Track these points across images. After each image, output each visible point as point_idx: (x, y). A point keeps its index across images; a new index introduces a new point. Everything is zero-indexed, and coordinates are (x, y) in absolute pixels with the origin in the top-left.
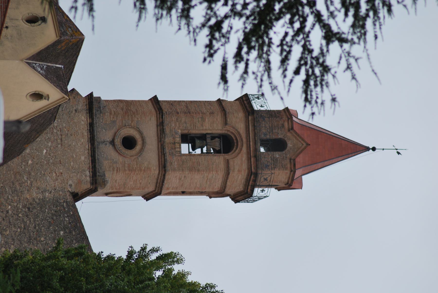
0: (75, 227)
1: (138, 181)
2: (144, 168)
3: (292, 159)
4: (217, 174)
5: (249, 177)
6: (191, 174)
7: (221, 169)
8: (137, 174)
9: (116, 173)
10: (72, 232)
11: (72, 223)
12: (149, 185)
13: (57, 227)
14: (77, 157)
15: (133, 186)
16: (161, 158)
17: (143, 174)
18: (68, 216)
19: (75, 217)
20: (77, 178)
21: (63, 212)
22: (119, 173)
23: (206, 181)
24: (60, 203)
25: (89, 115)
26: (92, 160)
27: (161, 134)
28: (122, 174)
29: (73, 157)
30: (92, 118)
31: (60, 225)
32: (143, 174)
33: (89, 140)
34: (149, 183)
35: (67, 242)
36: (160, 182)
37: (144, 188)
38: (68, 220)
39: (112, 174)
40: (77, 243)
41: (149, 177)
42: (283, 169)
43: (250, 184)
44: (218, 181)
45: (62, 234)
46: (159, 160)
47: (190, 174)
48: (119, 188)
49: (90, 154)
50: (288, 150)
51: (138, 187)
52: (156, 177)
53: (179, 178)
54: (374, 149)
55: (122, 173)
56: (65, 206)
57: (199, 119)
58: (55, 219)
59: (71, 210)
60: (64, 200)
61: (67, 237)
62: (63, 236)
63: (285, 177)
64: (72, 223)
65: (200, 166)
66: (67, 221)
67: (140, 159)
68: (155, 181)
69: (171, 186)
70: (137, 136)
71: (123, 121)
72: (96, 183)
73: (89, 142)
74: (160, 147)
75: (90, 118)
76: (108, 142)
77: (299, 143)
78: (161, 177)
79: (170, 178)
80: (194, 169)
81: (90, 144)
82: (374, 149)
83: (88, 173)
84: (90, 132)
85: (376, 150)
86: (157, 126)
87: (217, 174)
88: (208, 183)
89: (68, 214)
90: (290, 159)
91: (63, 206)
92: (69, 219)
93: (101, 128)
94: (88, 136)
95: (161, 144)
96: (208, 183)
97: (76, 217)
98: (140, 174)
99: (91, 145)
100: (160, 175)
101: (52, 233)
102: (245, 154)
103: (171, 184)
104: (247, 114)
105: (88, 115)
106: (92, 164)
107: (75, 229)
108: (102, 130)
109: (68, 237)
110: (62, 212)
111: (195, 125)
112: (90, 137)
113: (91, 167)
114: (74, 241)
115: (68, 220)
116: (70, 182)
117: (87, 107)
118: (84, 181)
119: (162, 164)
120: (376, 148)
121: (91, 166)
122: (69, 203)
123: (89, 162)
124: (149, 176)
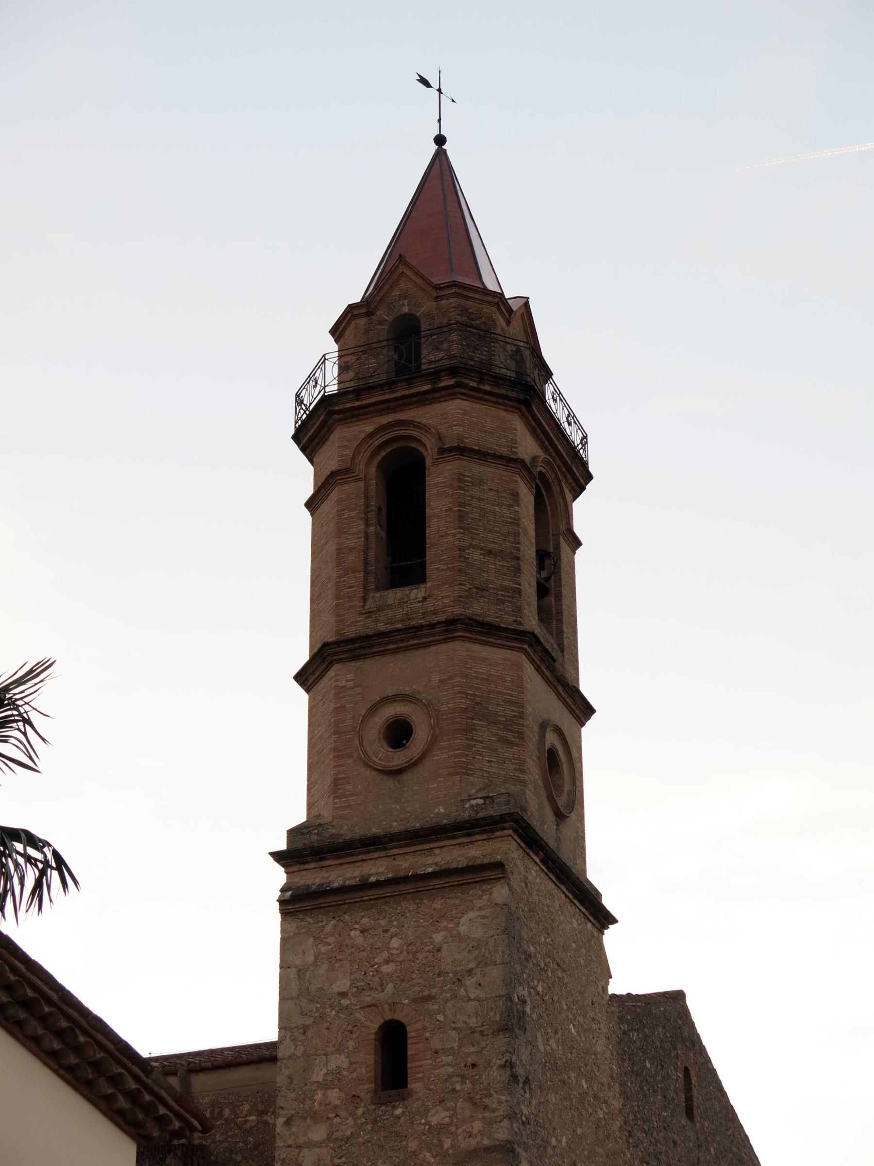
54: (440, 140)
82: (440, 140)
85: (442, 133)
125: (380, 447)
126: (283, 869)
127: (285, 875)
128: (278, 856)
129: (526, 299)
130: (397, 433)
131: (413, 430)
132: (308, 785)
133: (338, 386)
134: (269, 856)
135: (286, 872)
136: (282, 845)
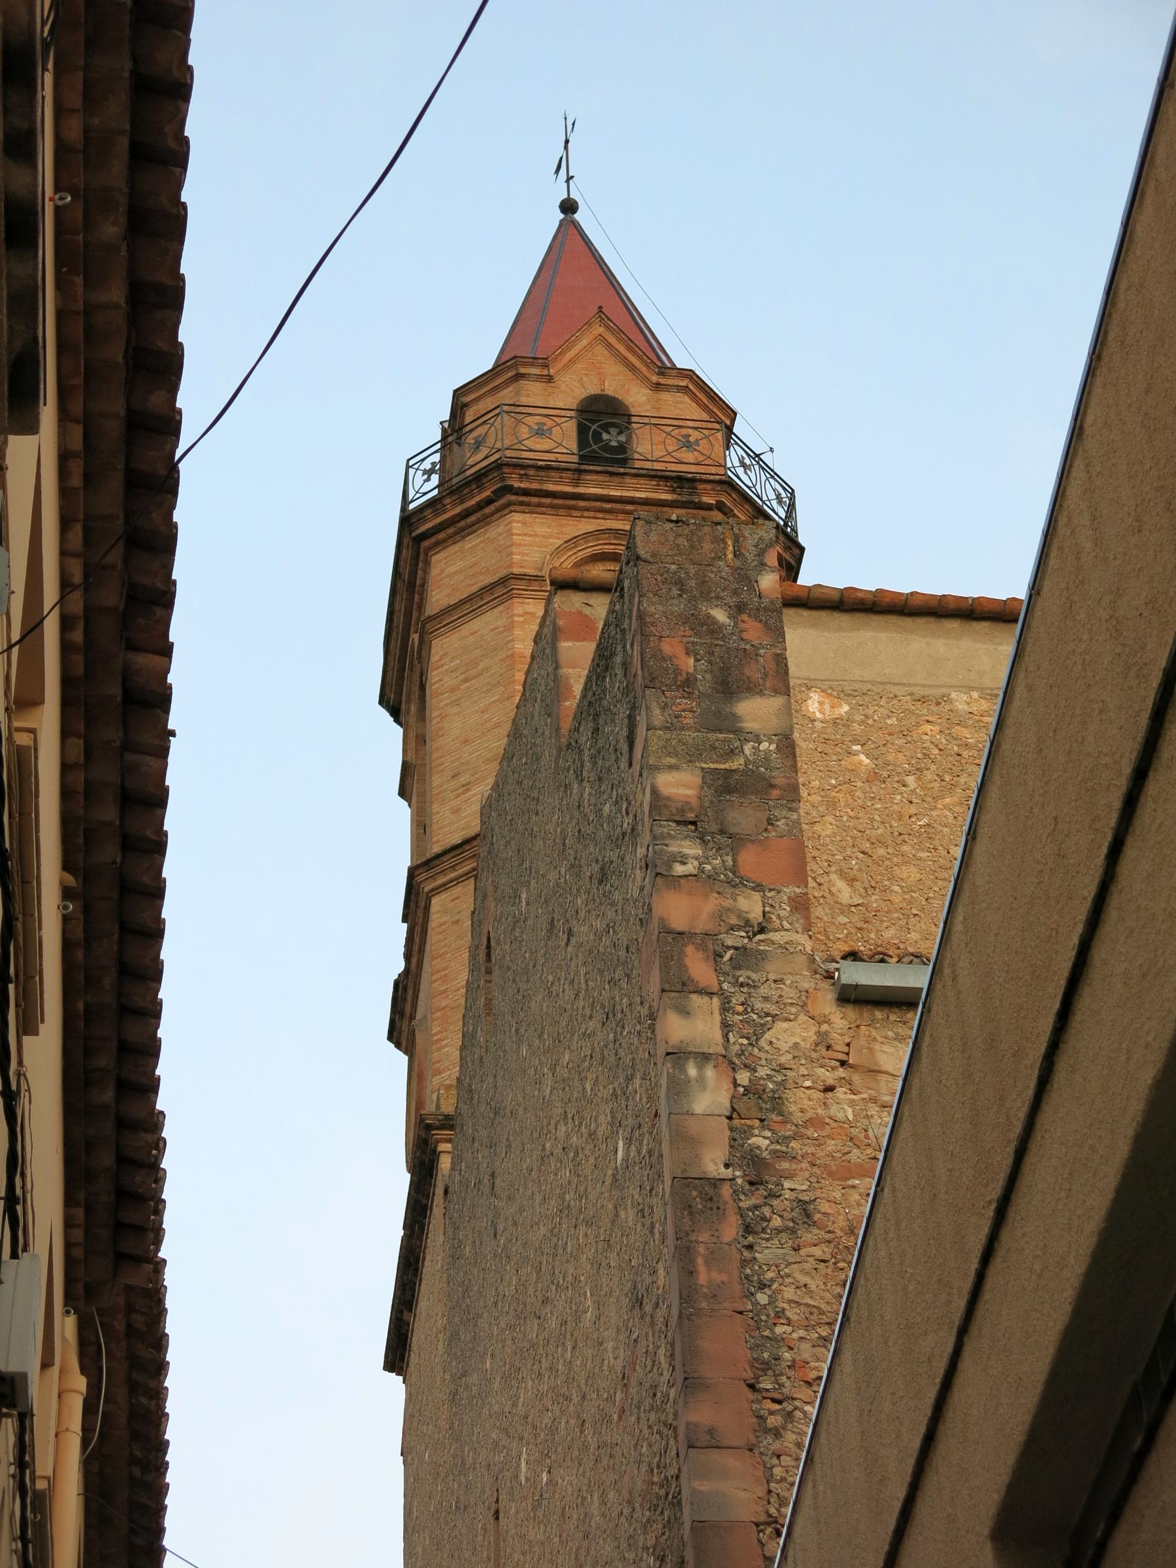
5: (441, 536)
17: (447, 953)
53: (463, 793)
54: (569, 207)
82: (569, 207)
98: (446, 969)
120: (566, 196)
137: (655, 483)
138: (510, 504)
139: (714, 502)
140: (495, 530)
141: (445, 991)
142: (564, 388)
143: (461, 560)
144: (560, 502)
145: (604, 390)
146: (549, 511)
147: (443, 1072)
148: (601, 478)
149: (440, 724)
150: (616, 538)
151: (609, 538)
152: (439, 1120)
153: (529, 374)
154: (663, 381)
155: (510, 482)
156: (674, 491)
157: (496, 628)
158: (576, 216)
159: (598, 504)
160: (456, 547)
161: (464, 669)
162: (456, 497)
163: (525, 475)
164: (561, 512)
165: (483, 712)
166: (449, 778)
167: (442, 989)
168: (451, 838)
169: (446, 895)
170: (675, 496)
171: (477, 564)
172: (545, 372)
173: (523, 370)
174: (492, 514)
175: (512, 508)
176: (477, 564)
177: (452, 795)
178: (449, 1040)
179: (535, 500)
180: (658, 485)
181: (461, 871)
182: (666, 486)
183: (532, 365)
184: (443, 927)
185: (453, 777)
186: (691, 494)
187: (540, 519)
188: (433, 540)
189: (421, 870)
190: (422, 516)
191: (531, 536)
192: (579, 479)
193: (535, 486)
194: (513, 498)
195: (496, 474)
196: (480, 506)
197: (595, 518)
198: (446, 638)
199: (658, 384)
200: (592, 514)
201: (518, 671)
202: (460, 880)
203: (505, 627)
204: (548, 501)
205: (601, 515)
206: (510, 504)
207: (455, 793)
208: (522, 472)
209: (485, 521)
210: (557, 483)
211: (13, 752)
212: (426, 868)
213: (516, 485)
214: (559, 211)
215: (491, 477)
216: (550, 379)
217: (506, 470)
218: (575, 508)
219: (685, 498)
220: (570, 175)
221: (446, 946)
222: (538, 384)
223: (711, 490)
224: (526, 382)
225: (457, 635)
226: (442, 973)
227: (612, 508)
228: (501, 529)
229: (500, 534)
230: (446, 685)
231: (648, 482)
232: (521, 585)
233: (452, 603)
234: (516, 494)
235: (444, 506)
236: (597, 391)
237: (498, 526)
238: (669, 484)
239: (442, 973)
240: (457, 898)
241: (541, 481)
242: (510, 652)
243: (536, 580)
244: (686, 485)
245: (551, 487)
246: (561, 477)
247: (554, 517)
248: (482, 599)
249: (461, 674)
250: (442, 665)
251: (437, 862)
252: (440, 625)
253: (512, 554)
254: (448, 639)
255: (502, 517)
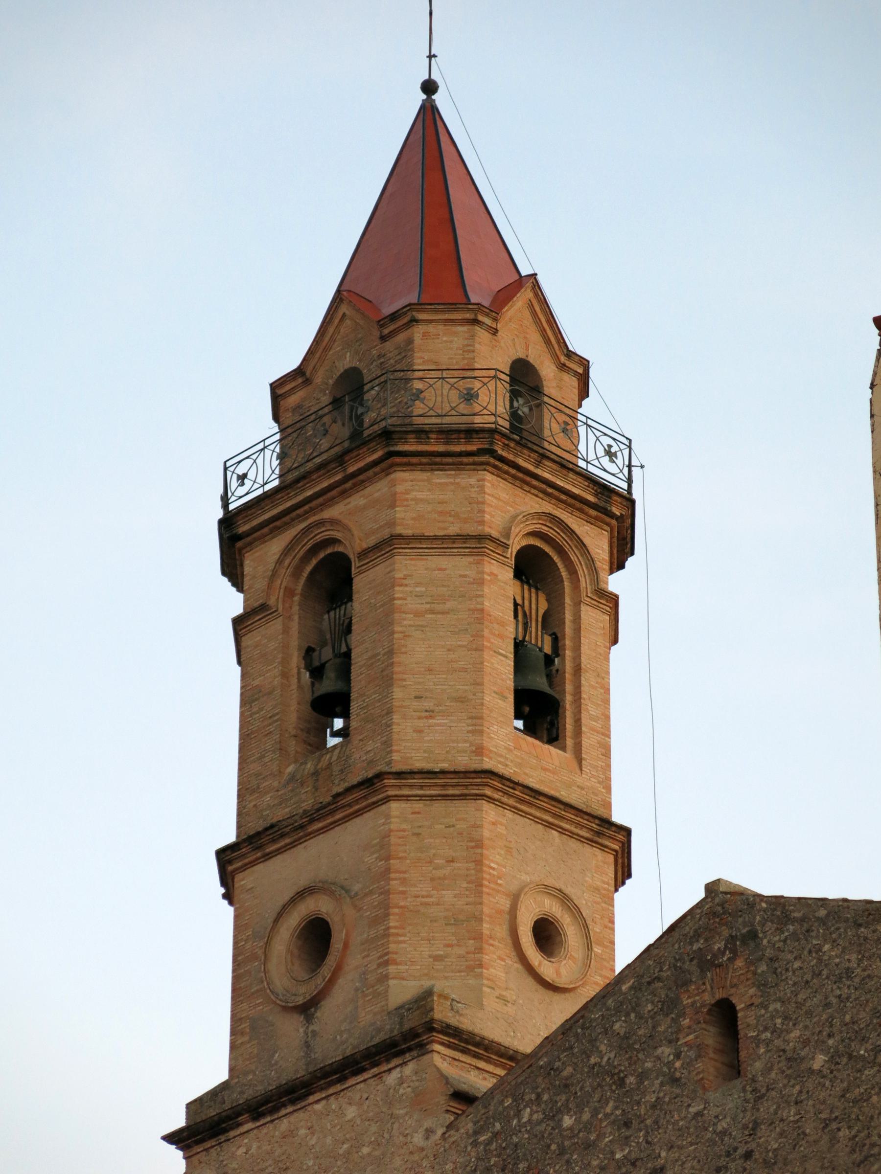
0: (549, 1074)
1: (440, 873)
2: (381, 860)
3: (381, 332)
4: (405, 582)
5: (414, 460)
6: (406, 676)
7: (388, 570)
8: (404, 881)
9: (396, 964)
10: (567, 1079)
11: (537, 1088)
12: (461, 826)
13: (549, 1146)
14: (348, 1136)
15: (465, 885)
16: (350, 805)
17: (406, 858)
18: (518, 1114)
19: (521, 1083)
20: (406, 1114)
21: (505, 1140)
22: (396, 953)
23: (443, 613)
24: (478, 1159)
25: (232, 1129)
26: (356, 1073)
27: (283, 836)
28: (404, 942)
29: (348, 1152)
30: (237, 1117)
31: (543, 1136)
32: (406, 858)
33: (299, 1106)
34: (452, 829)
35: (594, 1089)
36: (436, 785)
37: (473, 844)
38: (528, 1110)
39: (403, 979)
40: (598, 1048)
41: (418, 834)
42: (409, 353)
43: (441, 448)
44: (440, 569)
45: (571, 1116)
46: (357, 811)
47: (405, 680)
48: (471, 942)
49: (339, 1087)
50: (360, 360)
51: (472, 865)
52: (419, 806)
53: (426, 717)
54: (429, 87)
55: (395, 942)
56: (490, 1134)
57: (255, 710)
58: (526, 1165)
59: (501, 1109)
60: (469, 1148)
61: (579, 1094)
62: (575, 1113)
63: (445, 339)
64: (540, 1090)
65: (378, 654)
66: (532, 1110)
67: (356, 887)
68: (439, 807)
69: (465, 741)
70: (294, 920)
71: (253, 994)
72: (413, 1034)
73: (303, 1104)
74: (320, 825)
75: (239, 1125)
76: (307, 1028)
77: (342, 331)
78: (411, 786)
79: (425, 752)
80: (385, 673)
81: (311, 1099)
82: (429, 87)
83: (392, 1078)
84: (276, 1109)
85: (433, 77)
86: (268, 857)
87: (405, 582)
88: (449, 605)
89: (512, 1113)
90: (383, 338)
91: (488, 1143)
92: (525, 1107)
93: (268, 1072)
94: (291, 1113)
95: (312, 821)
96: (449, 605)
97: (519, 1080)
98: (404, 872)
99: (312, 1094)
100: (405, 792)
101: (568, 1162)
102: (349, 503)
103: (453, 741)
104: (239, 544)
105: (232, 1134)
106: (363, 1070)
107: (557, 1069)
108: (276, 1063)
109: (581, 1089)
110: (504, 1145)
111: (270, 717)
112: (293, 1102)
113: (375, 1070)
114: (593, 1060)
115: (528, 1110)
116: (418, 1139)
117: (213, 1147)
118: (417, 1084)
119: (365, 797)
120: (427, 77)
121: (372, 1071)
122: (478, 1122)
123: (362, 1085)
124: (414, 834)
125: (306, 558)
126: (180, 1154)
127: (184, 1161)
128: (172, 1138)
129: (532, 280)
130: (319, 538)
131: (332, 530)
132: (239, 791)
133: (281, 435)
134: (165, 1144)
135: (185, 1158)
136: (179, 1121)
137: (587, 484)
138: (488, 464)
139: (619, 514)
140: (468, 479)
141: (403, 893)
142: (502, 344)
143: (429, 490)
144: (521, 475)
145: (527, 356)
146: (510, 479)
147: (400, 964)
148: (555, 466)
149: (403, 641)
150: (551, 522)
151: (545, 521)
152: (442, 1027)
153: (483, 323)
154: (568, 363)
155: (496, 448)
156: (596, 495)
157: (465, 576)
158: (434, 97)
159: (544, 486)
160: (425, 475)
161: (429, 600)
162: (444, 436)
163: (507, 445)
164: (517, 483)
165: (449, 650)
166: (412, 697)
167: (401, 889)
168: (413, 755)
169: (407, 805)
170: (596, 500)
171: (446, 503)
172: (494, 326)
173: (480, 318)
174: (467, 464)
175: (488, 468)
176: (446, 503)
177: (414, 713)
178: (406, 939)
179: (506, 467)
180: (588, 487)
181: (428, 792)
182: (593, 489)
183: (487, 315)
184: (403, 833)
185: (415, 698)
186: (606, 502)
187: (502, 484)
188: (405, 460)
189: (391, 776)
190: (405, 436)
191: (496, 498)
192: (540, 462)
193: (511, 457)
194: (492, 460)
195: (487, 436)
196: (461, 454)
197: (537, 496)
198: (411, 559)
199: (564, 365)
200: (536, 492)
201: (487, 628)
202: (424, 798)
203: (474, 579)
204: (513, 471)
205: (541, 495)
206: (488, 464)
207: (418, 714)
208: (507, 442)
209: (459, 467)
210: (525, 460)
211: (555, 815)
212: (395, 776)
213: (500, 452)
214: (420, 86)
215: (481, 436)
216: (495, 332)
217: (497, 437)
218: (528, 484)
219: (602, 504)
220: (432, 54)
221: (405, 851)
222: (486, 334)
223: (621, 503)
224: (479, 329)
225: (423, 563)
226: (402, 875)
227: (552, 493)
228: (473, 481)
229: (472, 486)
230: (410, 606)
231: (582, 481)
232: (491, 546)
233: (426, 534)
234: (494, 458)
235: (428, 438)
236: (524, 357)
237: (470, 477)
238: (595, 488)
239: (402, 875)
240: (419, 813)
241: (516, 455)
242: (479, 607)
243: (502, 546)
244: (606, 493)
245: (521, 462)
246: (529, 456)
247: (510, 485)
248: (454, 543)
249: (427, 603)
250: (406, 585)
251: (408, 776)
252: (406, 546)
253: (484, 512)
254: (413, 562)
255: (474, 470)
